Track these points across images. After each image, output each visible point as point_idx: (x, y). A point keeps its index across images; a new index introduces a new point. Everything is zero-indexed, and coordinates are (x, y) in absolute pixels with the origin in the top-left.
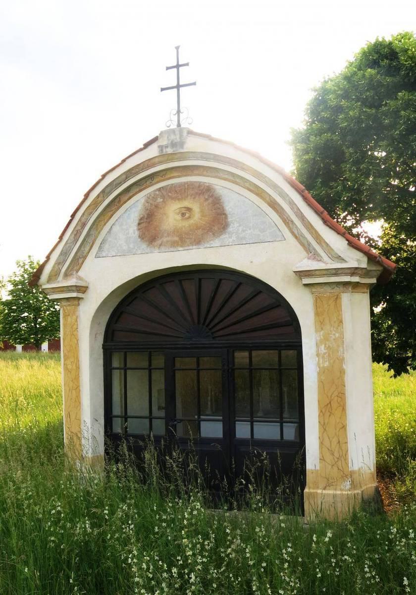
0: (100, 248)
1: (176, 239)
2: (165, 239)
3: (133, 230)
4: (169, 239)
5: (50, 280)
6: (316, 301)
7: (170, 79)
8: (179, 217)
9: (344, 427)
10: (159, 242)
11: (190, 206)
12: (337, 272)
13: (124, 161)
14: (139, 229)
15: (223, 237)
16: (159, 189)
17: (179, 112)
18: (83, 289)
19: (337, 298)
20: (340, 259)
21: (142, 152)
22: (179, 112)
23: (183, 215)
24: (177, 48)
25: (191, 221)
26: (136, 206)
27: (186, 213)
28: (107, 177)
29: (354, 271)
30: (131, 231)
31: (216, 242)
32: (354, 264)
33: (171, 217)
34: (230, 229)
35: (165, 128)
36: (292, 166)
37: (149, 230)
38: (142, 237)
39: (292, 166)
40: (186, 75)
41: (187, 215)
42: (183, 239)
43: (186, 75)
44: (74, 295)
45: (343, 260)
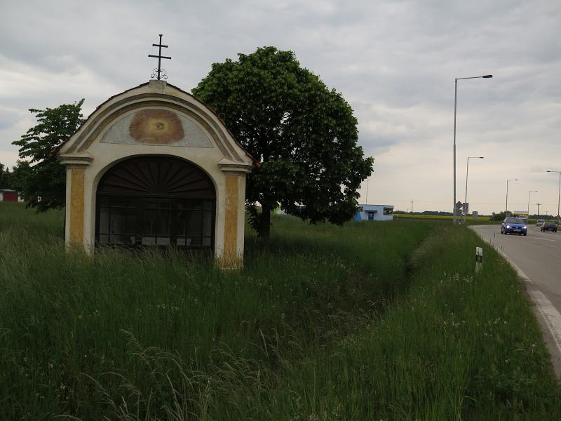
0: (103, 137)
1: (153, 139)
2: (146, 138)
3: (126, 131)
4: (149, 138)
5: (68, 152)
6: (226, 179)
7: (156, 51)
8: (156, 127)
9: (236, 238)
10: (142, 139)
11: (162, 122)
12: (239, 166)
13: (126, 92)
14: (130, 130)
15: (180, 142)
16: (144, 110)
17: (159, 71)
18: (90, 160)
19: (236, 178)
20: (241, 160)
21: (138, 89)
22: (159, 71)
23: (158, 126)
24: (161, 36)
25: (163, 131)
26: (130, 116)
27: (160, 126)
28: (114, 99)
29: (246, 167)
30: (125, 131)
31: (177, 144)
32: (247, 164)
33: (151, 126)
34: (185, 138)
35: (71, 104)
36: (8, 169)
37: (137, 132)
38: (132, 135)
39: (8, 169)
40: (164, 52)
41: (161, 127)
42: (158, 140)
43: (164, 52)
44: (86, 163)
45: (243, 162)
